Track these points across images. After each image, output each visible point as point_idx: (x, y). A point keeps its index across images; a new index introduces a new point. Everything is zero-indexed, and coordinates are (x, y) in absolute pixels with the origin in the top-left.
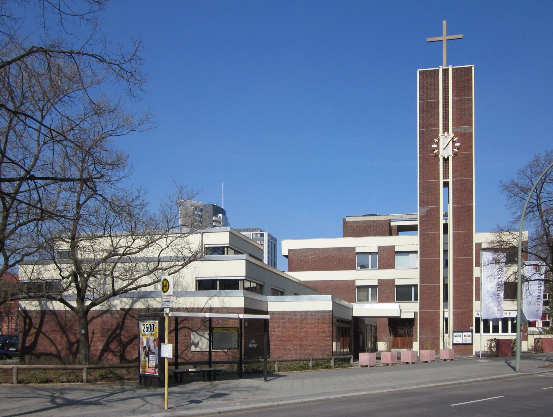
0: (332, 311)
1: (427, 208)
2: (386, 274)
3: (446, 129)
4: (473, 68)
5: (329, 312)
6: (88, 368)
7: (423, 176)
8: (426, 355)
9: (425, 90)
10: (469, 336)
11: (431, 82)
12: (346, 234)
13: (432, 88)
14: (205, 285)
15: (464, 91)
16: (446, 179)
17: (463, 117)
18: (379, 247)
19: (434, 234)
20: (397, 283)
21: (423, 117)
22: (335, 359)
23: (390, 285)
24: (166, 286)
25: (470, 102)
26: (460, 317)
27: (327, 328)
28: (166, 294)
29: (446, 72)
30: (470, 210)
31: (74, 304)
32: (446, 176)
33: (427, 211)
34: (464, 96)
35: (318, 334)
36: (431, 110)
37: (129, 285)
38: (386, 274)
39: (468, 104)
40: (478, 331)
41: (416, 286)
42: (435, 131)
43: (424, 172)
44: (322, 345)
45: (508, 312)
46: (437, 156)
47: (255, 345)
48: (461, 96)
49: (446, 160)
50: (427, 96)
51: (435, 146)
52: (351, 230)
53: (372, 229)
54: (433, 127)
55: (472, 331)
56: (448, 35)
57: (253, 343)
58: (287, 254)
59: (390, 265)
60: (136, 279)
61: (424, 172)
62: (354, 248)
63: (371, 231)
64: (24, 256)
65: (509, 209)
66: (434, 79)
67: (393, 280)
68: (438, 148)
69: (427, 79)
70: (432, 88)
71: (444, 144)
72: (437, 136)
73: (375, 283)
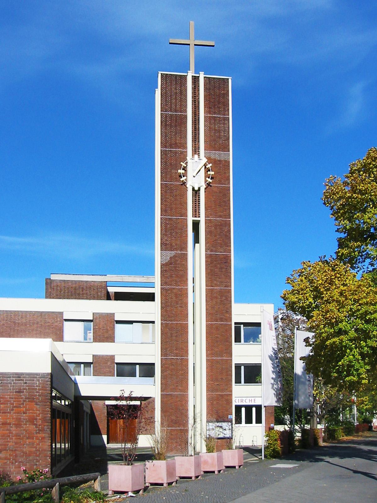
0: (51, 374)
1: (170, 254)
3: (196, 151)
4: (230, 81)
5: (43, 376)
7: (166, 211)
8: (210, 461)
9: (169, 99)
11: (176, 89)
12: (49, 295)
13: (178, 98)
15: (219, 108)
17: (217, 141)
19: (181, 290)
20: (117, 360)
21: (166, 133)
22: (61, 486)
25: (226, 122)
26: (215, 403)
27: (41, 413)
29: (195, 80)
30: (226, 260)
32: (196, 212)
33: (171, 258)
34: (219, 114)
35: (18, 425)
36: (176, 126)
38: (103, 349)
39: (224, 124)
40: (238, 421)
43: (166, 205)
44: (26, 449)
45: (253, 399)
46: (184, 183)
48: (215, 113)
49: (196, 192)
50: (171, 107)
51: (181, 171)
52: (55, 291)
53: (84, 292)
54: (179, 148)
55: (231, 422)
56: (196, 38)
59: (110, 338)
61: (166, 205)
63: (83, 294)
66: (181, 87)
68: (185, 175)
69: (171, 85)
70: (178, 98)
71: (194, 170)
72: (184, 159)
73: (91, 360)
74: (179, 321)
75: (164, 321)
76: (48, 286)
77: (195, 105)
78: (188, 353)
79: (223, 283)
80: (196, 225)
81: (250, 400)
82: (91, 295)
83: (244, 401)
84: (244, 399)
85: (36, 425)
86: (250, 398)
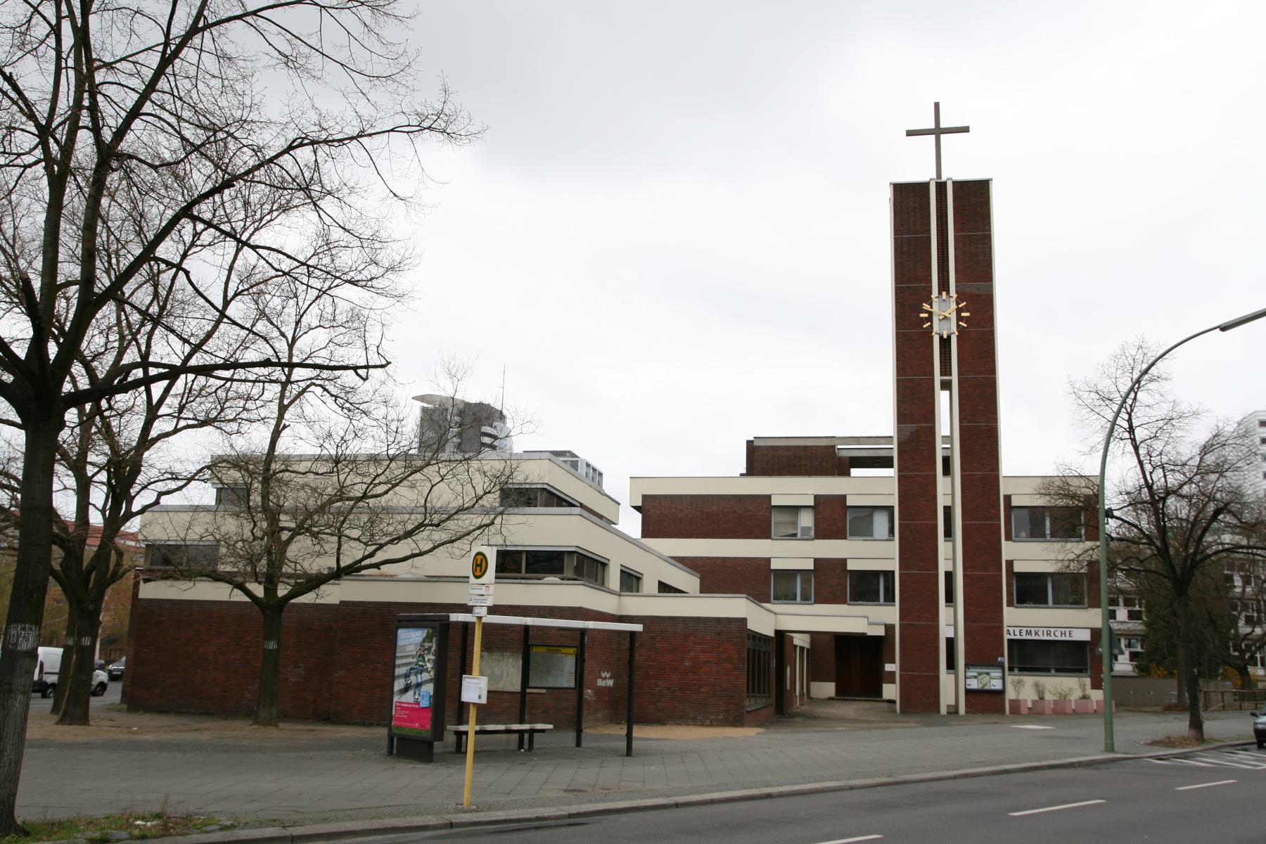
1: (912, 427)
2: (831, 549)
3: (944, 286)
6: (477, 733)
14: (514, 564)
18: (816, 497)
20: (851, 566)
23: (838, 571)
24: (480, 565)
28: (481, 581)
31: (259, 590)
37: (365, 558)
38: (831, 549)
41: (889, 575)
42: (924, 289)
47: (610, 683)
49: (945, 343)
57: (605, 678)
58: (640, 504)
60: (381, 546)
62: (769, 497)
64: (161, 494)
65: (1224, 462)
67: (844, 561)
68: (930, 319)
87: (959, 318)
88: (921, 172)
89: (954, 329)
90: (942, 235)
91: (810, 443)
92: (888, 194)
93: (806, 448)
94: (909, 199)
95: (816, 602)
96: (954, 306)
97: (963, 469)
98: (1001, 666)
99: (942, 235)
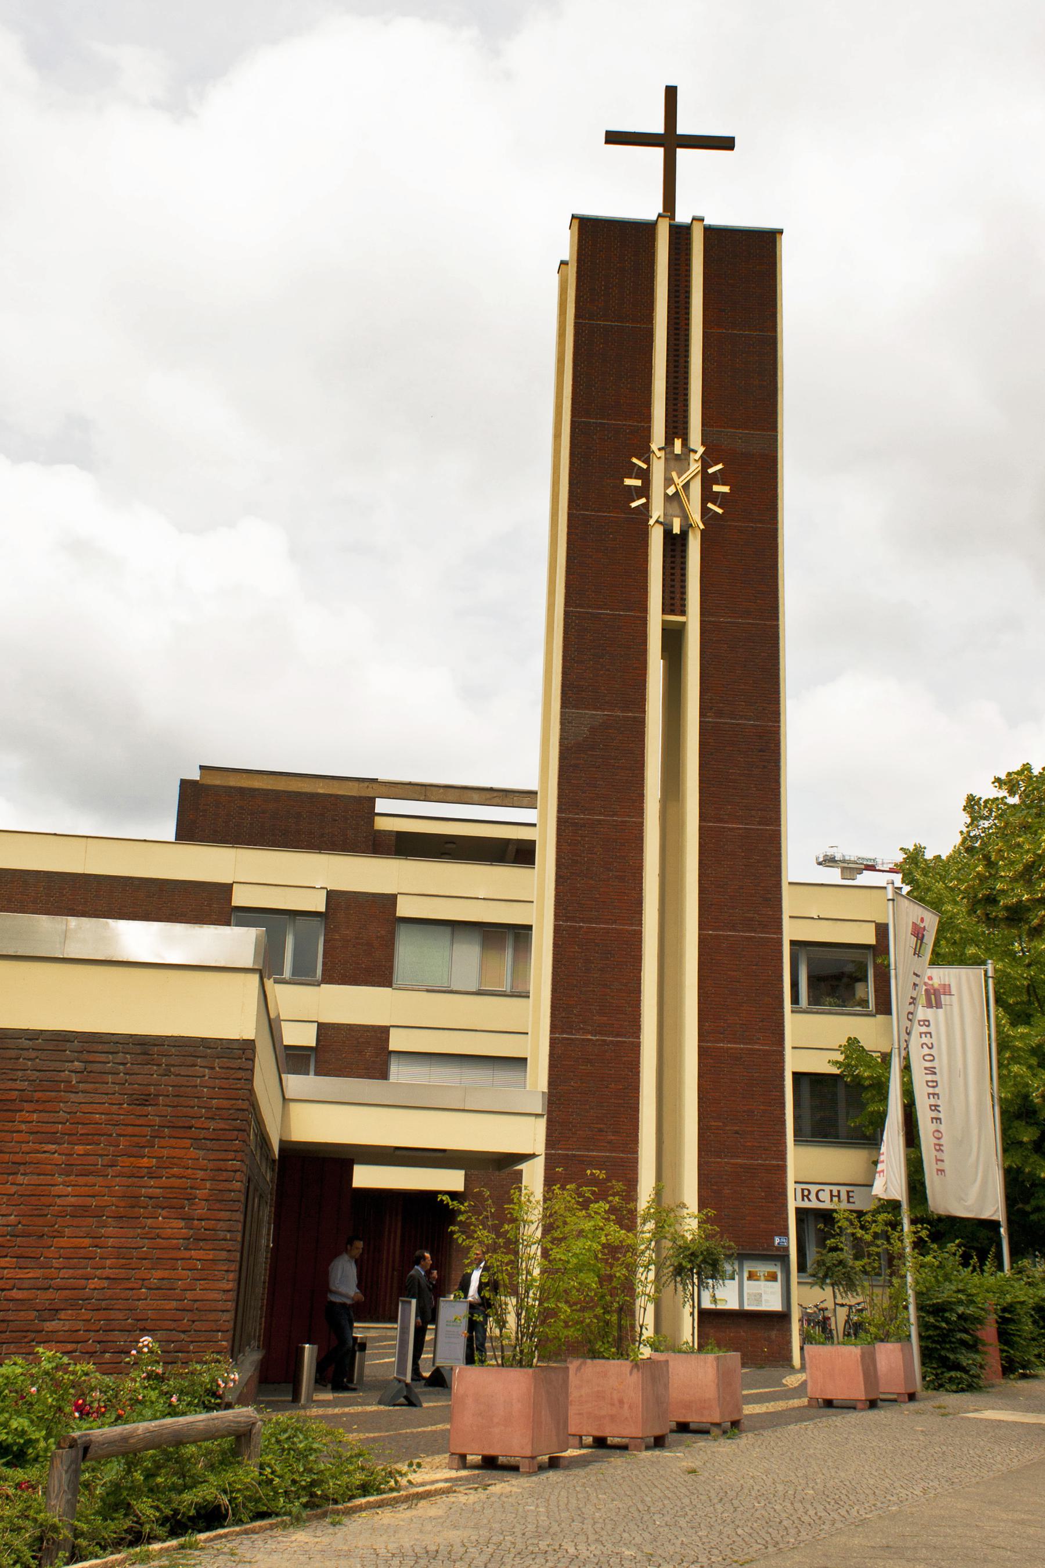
10: (773, 1278)
16: (672, 612)
32: (674, 601)
49: (675, 545)
68: (645, 491)
74: (615, 922)
75: (566, 921)
76: (837, 872)
77: (676, 361)
78: (640, 1026)
79: (753, 813)
80: (673, 638)
81: (835, 1193)
82: (322, 836)
83: (813, 1196)
84: (814, 1189)
85: (188, 1219)
86: (835, 1189)
87: (707, 496)
88: (641, 204)
89: (696, 517)
90: (671, 341)
91: (321, 789)
92: (563, 245)
93: (313, 797)
94: (608, 256)
95: (329, 978)
96: (695, 467)
97: (703, 817)
98: (782, 1258)
99: (671, 341)
